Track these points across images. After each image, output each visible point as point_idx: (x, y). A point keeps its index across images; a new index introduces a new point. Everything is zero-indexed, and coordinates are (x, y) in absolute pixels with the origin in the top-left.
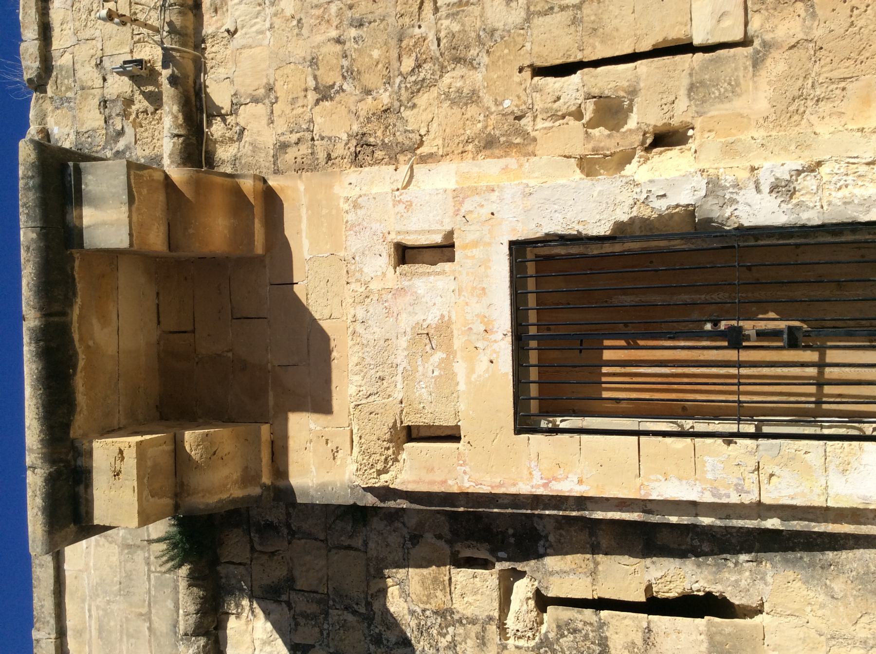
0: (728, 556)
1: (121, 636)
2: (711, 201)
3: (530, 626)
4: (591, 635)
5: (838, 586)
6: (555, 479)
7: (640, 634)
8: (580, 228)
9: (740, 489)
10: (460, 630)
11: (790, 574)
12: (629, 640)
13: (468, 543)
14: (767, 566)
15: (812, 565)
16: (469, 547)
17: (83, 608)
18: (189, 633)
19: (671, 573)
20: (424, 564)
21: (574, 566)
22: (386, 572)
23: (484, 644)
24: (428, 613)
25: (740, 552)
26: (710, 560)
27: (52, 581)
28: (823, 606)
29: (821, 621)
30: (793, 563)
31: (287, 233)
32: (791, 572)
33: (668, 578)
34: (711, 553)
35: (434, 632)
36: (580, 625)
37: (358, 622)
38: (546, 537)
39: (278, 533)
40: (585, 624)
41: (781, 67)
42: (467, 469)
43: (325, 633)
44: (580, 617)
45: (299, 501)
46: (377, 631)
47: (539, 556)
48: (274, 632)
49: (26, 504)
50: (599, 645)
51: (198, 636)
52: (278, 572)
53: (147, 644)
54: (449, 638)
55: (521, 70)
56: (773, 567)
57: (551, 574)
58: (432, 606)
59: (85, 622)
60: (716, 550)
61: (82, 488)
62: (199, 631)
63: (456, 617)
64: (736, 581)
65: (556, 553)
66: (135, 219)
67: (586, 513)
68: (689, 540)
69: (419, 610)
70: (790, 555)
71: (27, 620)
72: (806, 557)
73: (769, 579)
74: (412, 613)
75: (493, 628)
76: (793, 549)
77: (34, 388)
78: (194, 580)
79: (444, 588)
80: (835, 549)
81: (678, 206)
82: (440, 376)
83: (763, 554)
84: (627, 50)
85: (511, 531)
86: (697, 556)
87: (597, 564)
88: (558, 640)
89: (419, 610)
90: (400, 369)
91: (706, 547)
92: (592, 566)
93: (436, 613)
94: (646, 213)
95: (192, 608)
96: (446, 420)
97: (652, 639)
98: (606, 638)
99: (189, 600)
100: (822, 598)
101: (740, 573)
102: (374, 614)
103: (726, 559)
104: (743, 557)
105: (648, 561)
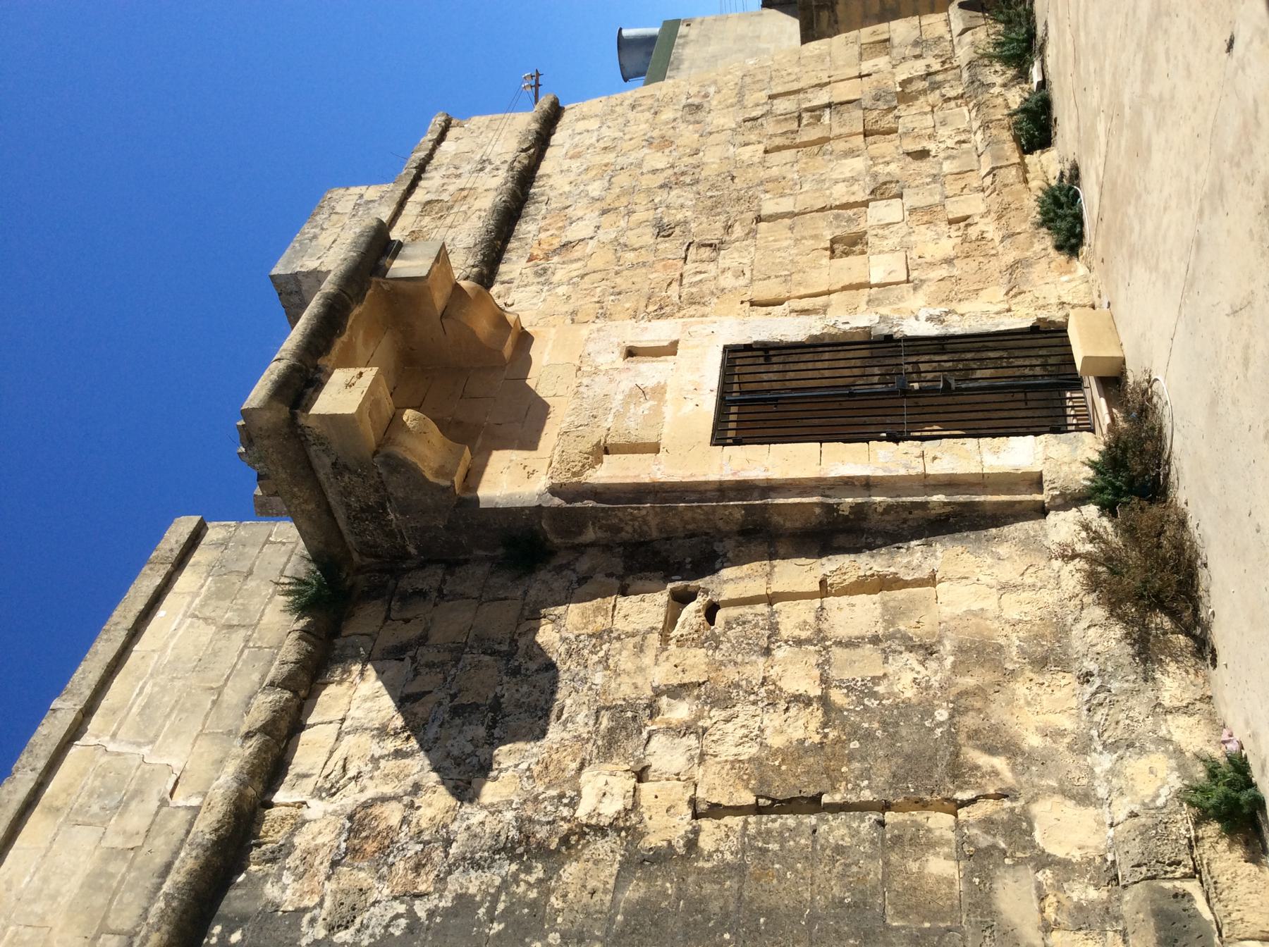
0: (901, 545)
1: (172, 710)
2: (882, 325)
3: (696, 627)
4: (761, 623)
5: (1003, 550)
6: (743, 470)
7: (813, 614)
8: (782, 338)
9: (907, 467)
10: (617, 645)
11: (959, 549)
12: (801, 619)
13: (641, 575)
14: (938, 547)
15: (978, 540)
16: (641, 579)
17: (134, 687)
18: (277, 682)
19: (846, 566)
20: (588, 598)
21: (750, 572)
22: (543, 611)
23: (642, 651)
24: (582, 637)
25: (912, 539)
26: (883, 550)
27: (112, 655)
28: (990, 567)
29: (990, 577)
30: (961, 541)
31: (531, 353)
32: (959, 547)
33: (844, 571)
34: (885, 545)
35: (586, 652)
36: (750, 618)
37: (496, 660)
38: (725, 555)
39: (425, 598)
40: (756, 615)
41: (933, 288)
42: (662, 467)
43: (449, 679)
44: (752, 611)
45: (528, 382)
46: (516, 664)
47: (715, 571)
48: (383, 688)
49: (256, 383)
50: (769, 629)
51: (285, 689)
52: (411, 632)
53: (203, 717)
54: (602, 654)
55: (742, 302)
56: (942, 545)
57: (725, 582)
58: (590, 630)
59: (129, 700)
60: (889, 542)
61: (311, 390)
62: (286, 683)
63: (614, 635)
64: (908, 562)
65: (733, 564)
66: (435, 269)
67: (770, 501)
68: (863, 539)
69: (572, 637)
70: (957, 535)
71: (58, 687)
72: (972, 535)
73: (939, 554)
74: (564, 640)
75: (654, 639)
76: (960, 531)
77: (309, 320)
78: (306, 634)
79: (607, 613)
80: (997, 526)
81: (857, 328)
82: (649, 414)
83: (931, 538)
84: (824, 288)
85: (689, 560)
86: (871, 549)
87: (773, 567)
88: (725, 633)
89: (572, 637)
90: (613, 411)
91: (879, 542)
92: (768, 568)
93: (590, 636)
94: (834, 331)
95: (292, 657)
96: (649, 436)
97: (825, 615)
98: (777, 623)
99: (293, 649)
100: (989, 561)
101: (911, 555)
102: (518, 649)
103: (899, 548)
104: (913, 543)
105: (824, 560)
